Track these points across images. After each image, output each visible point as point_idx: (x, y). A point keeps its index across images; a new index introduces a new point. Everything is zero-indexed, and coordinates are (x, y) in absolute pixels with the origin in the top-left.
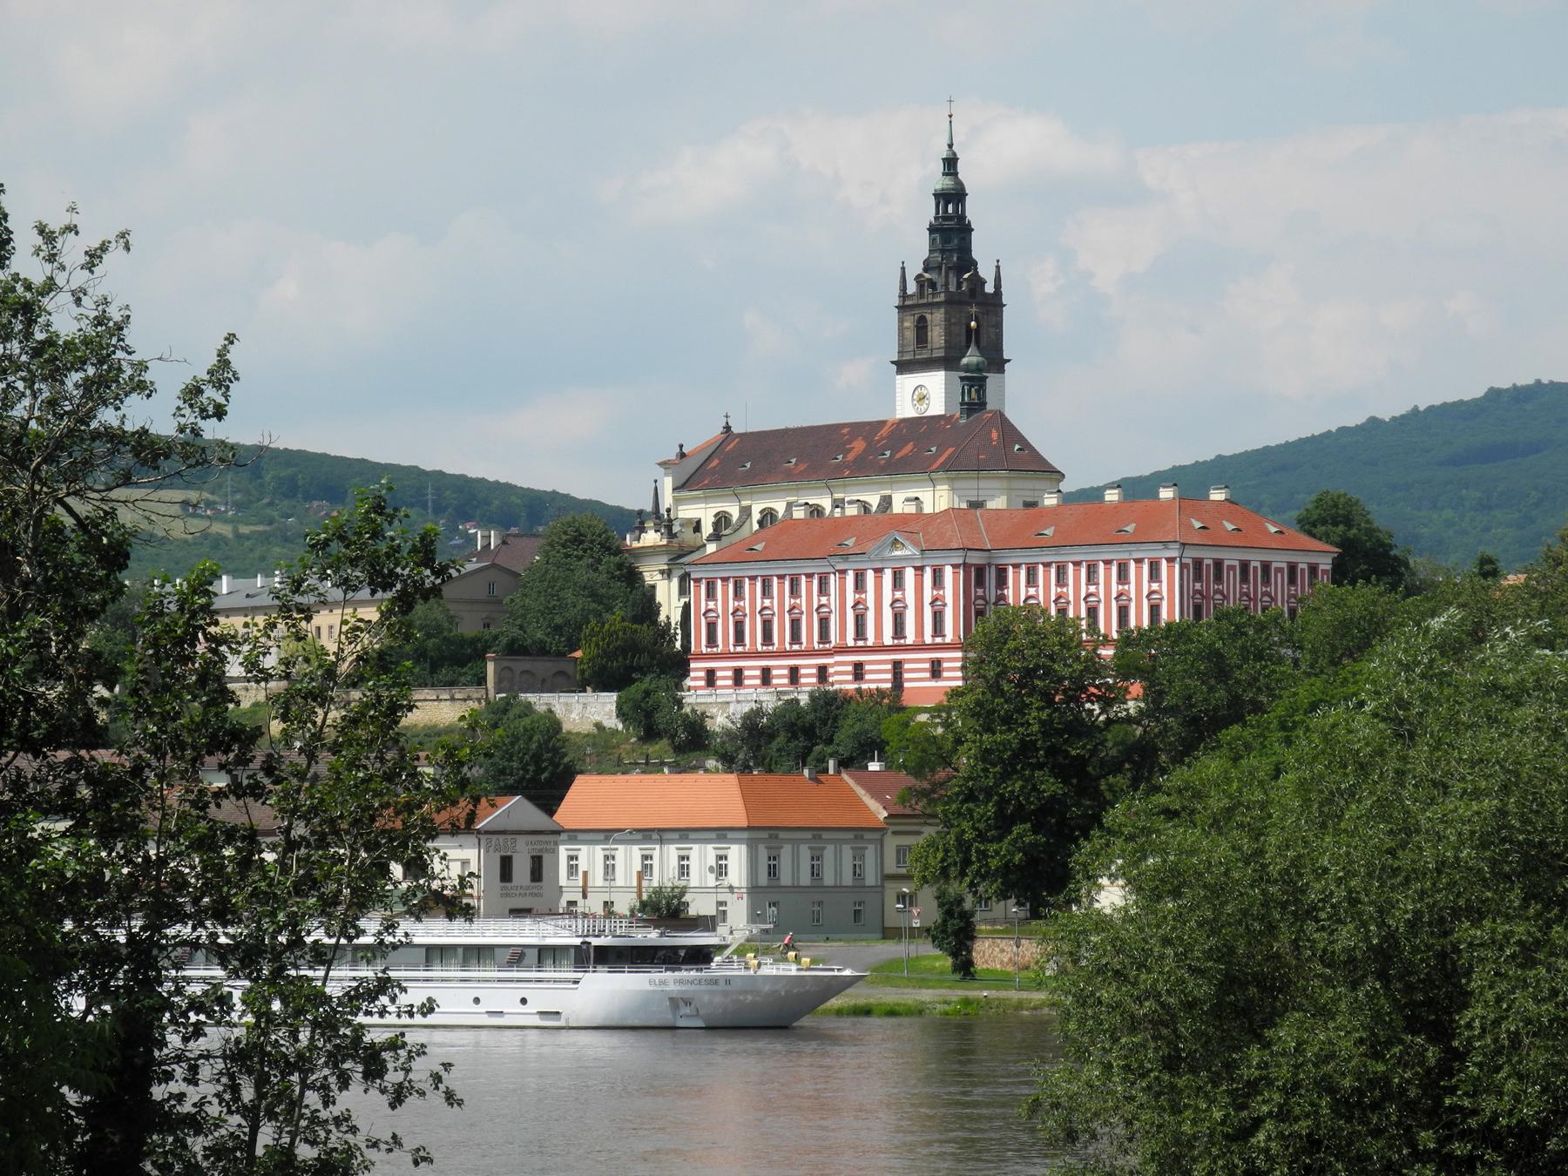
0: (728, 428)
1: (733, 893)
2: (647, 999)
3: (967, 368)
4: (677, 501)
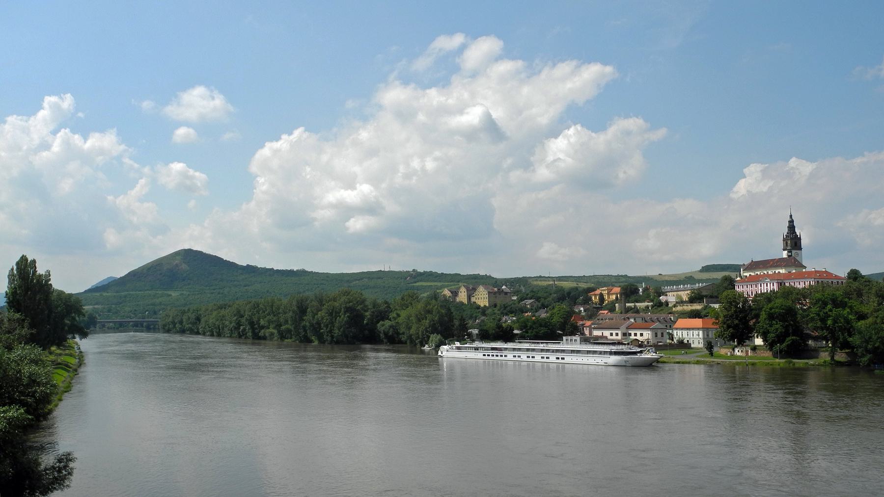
2: (621, 360)
3: (788, 250)
4: (743, 273)
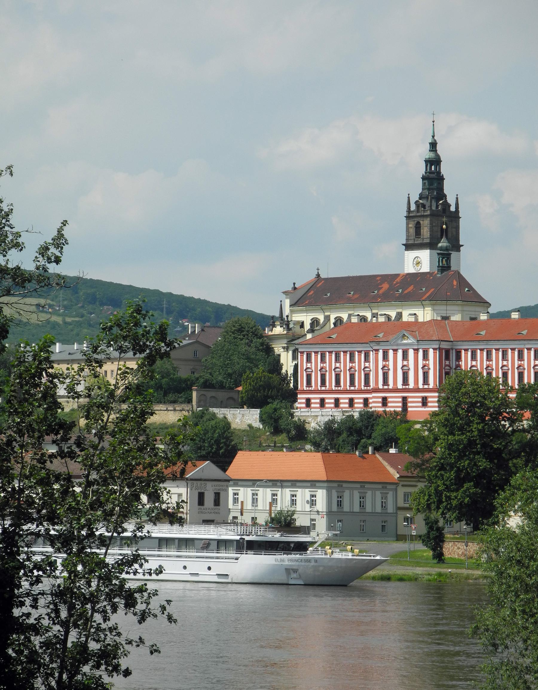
0: (318, 275)
1: (319, 514)
2: (274, 569)
3: (441, 249)
4: (292, 312)
